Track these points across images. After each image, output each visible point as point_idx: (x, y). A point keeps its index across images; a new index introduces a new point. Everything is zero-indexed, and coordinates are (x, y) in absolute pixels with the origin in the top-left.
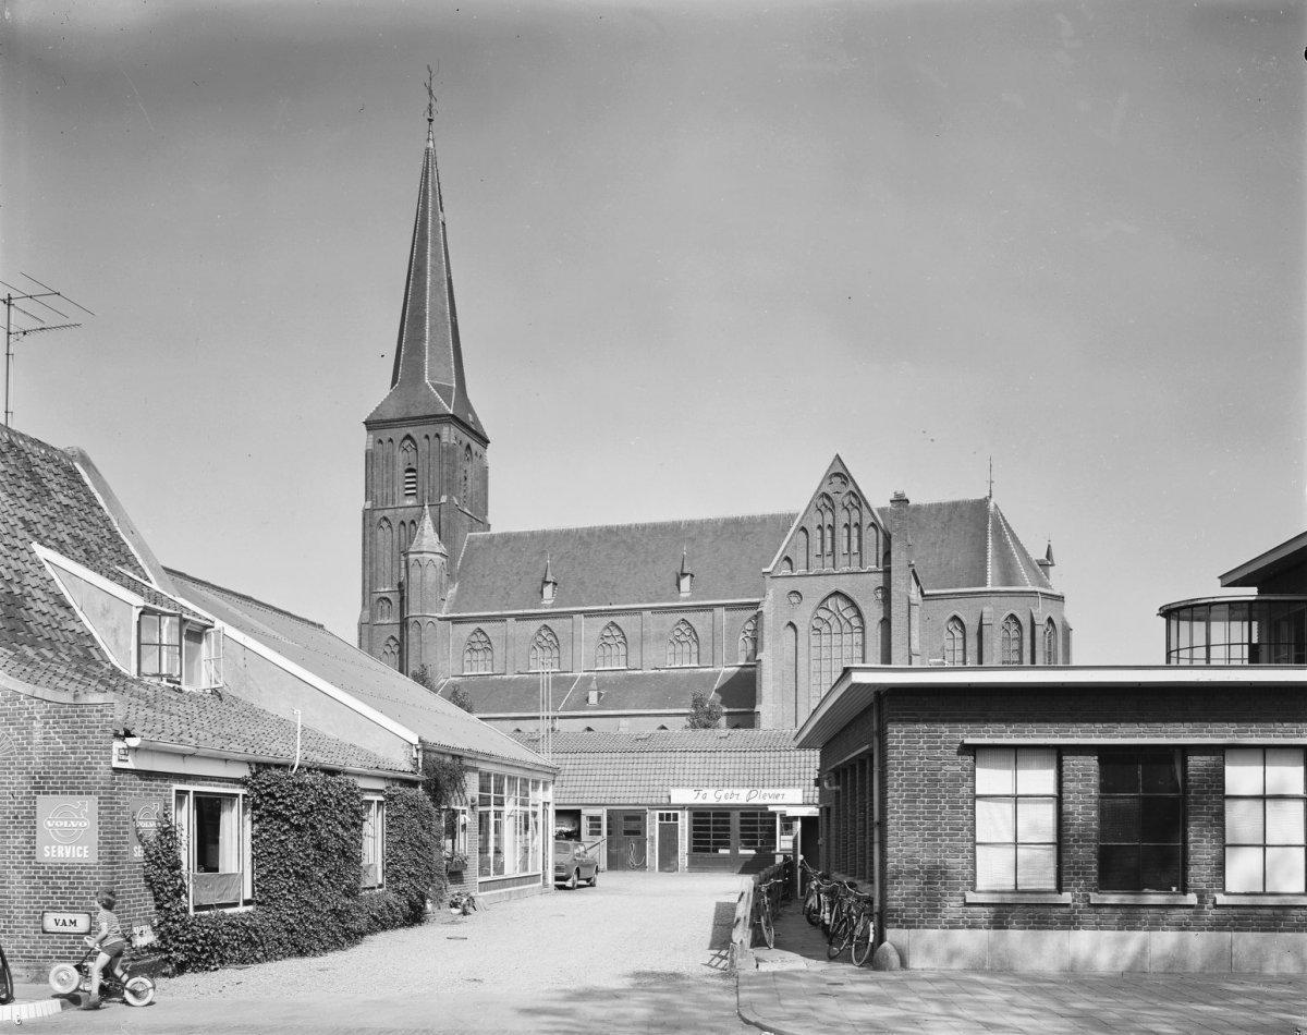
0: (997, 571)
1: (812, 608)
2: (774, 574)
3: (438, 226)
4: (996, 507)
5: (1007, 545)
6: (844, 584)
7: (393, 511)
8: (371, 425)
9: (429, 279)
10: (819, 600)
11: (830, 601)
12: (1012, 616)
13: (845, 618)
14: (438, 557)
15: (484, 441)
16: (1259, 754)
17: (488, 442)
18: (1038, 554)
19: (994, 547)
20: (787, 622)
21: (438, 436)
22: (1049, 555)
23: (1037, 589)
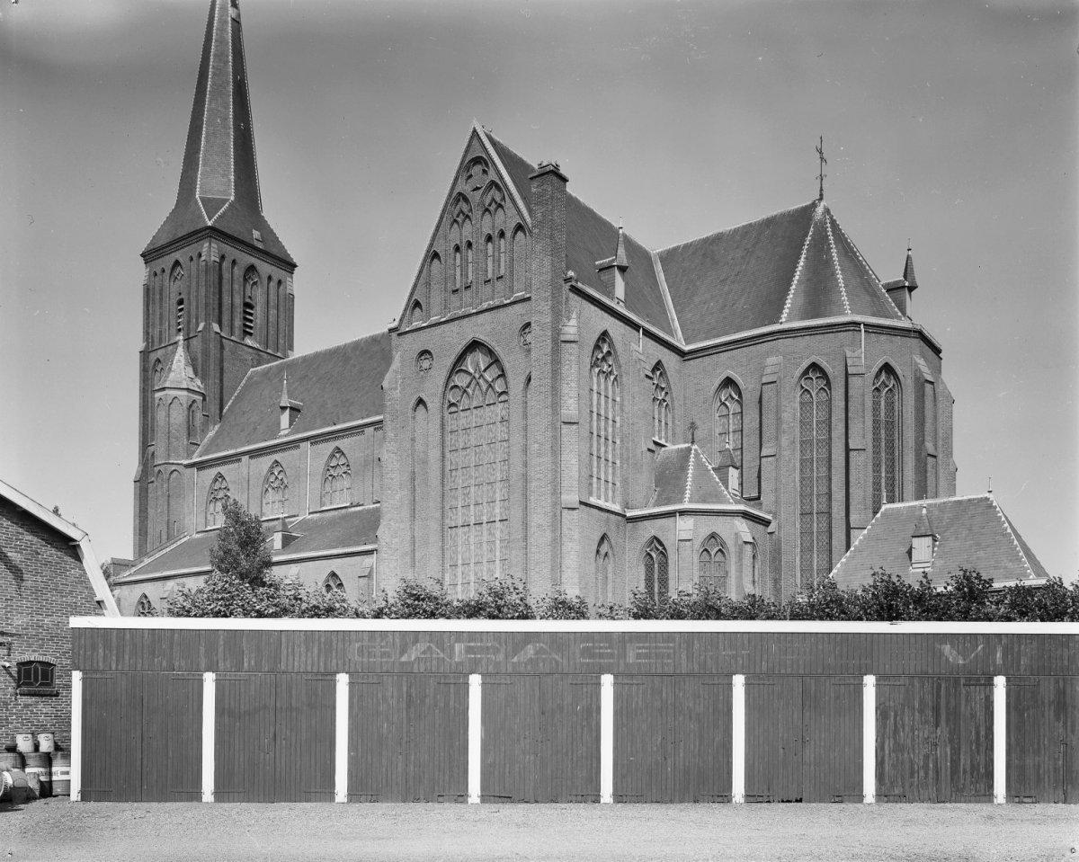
0: (801, 301)
1: (445, 373)
2: (402, 330)
3: (226, 22)
4: (827, 211)
5: (829, 262)
6: (478, 329)
7: (163, 350)
8: (149, 256)
9: (209, 83)
10: (452, 359)
11: (469, 359)
12: (814, 367)
13: (486, 381)
14: (185, 393)
15: (290, 266)
16: (838, 601)
17: (295, 266)
18: (888, 273)
19: (806, 267)
20: (413, 401)
21: (280, 282)
22: (907, 272)
23: (858, 318)
